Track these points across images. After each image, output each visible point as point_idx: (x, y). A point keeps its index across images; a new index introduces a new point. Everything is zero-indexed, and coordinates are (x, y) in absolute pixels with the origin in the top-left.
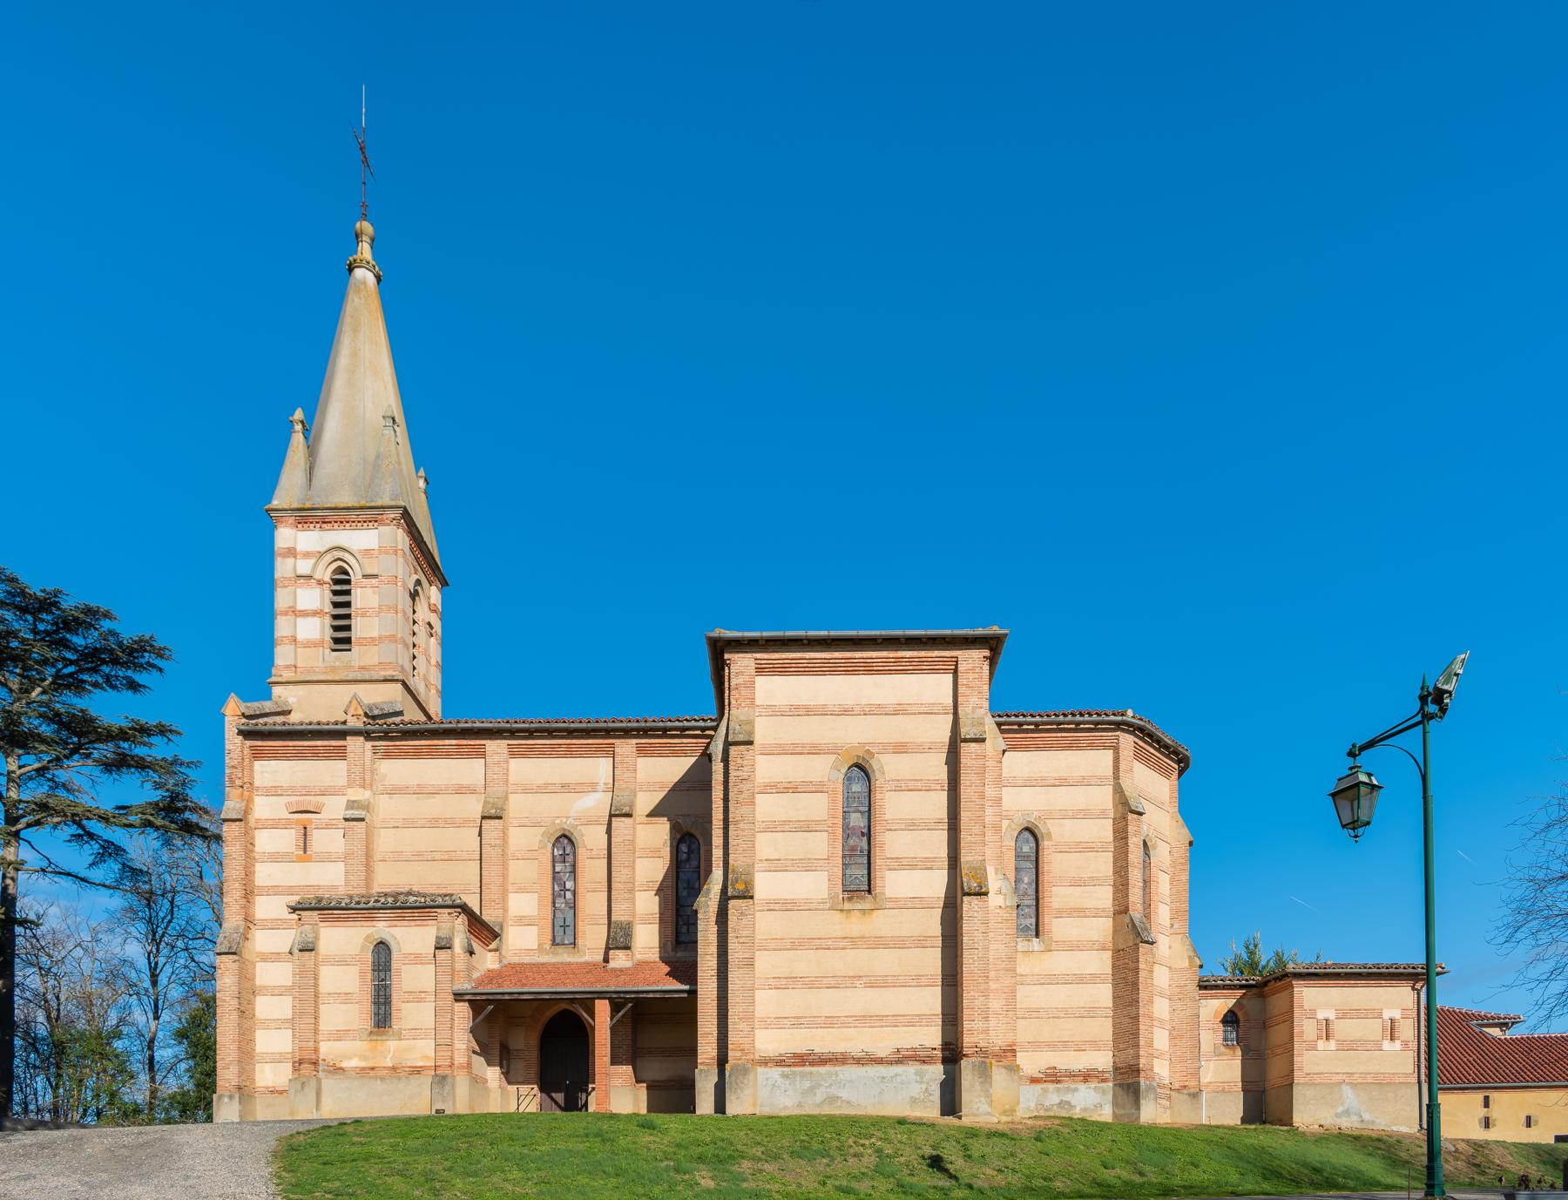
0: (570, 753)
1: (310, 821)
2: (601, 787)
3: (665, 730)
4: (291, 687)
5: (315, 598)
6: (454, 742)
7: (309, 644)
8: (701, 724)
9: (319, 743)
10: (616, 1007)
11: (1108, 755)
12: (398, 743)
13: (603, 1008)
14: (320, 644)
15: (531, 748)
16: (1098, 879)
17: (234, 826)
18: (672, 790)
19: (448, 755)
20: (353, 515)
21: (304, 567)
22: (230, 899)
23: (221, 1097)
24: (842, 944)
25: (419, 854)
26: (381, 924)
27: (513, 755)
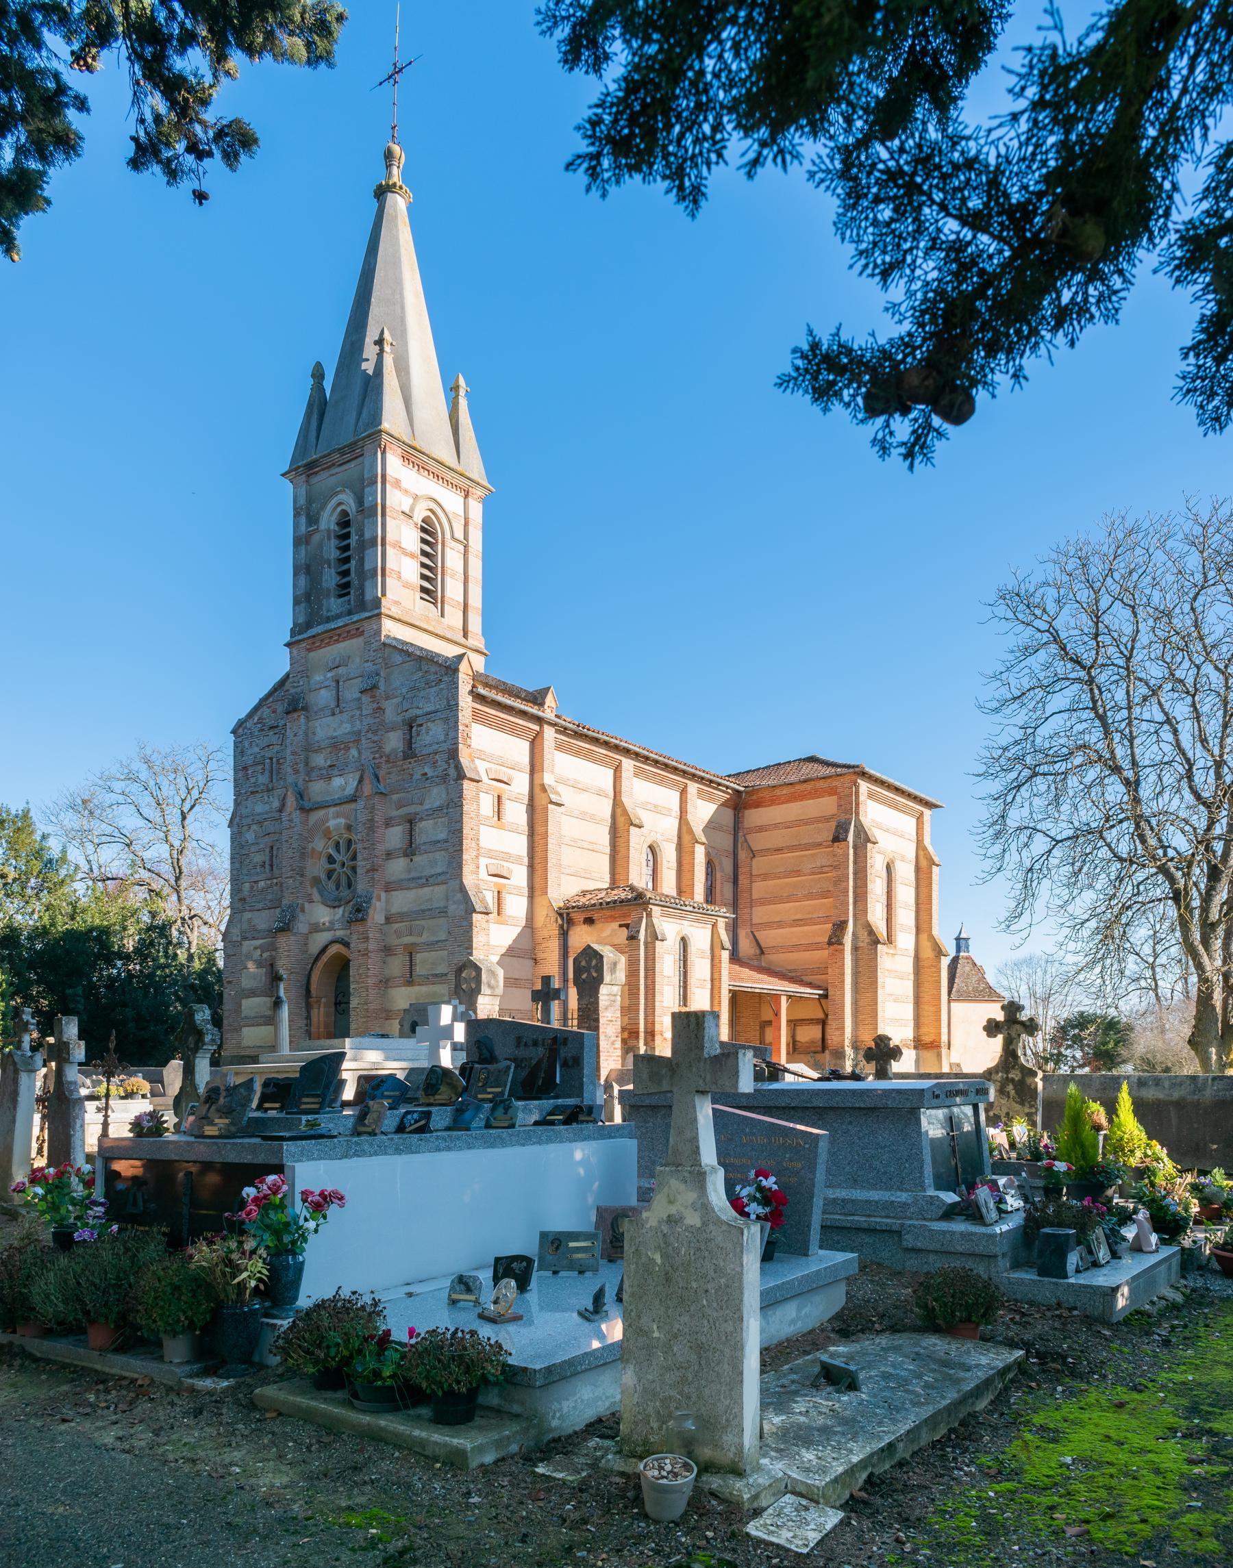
3: (711, 781)
4: (399, 625)
9: (521, 722)
13: (784, 999)
19: (594, 760)
20: (449, 475)
27: (636, 775)
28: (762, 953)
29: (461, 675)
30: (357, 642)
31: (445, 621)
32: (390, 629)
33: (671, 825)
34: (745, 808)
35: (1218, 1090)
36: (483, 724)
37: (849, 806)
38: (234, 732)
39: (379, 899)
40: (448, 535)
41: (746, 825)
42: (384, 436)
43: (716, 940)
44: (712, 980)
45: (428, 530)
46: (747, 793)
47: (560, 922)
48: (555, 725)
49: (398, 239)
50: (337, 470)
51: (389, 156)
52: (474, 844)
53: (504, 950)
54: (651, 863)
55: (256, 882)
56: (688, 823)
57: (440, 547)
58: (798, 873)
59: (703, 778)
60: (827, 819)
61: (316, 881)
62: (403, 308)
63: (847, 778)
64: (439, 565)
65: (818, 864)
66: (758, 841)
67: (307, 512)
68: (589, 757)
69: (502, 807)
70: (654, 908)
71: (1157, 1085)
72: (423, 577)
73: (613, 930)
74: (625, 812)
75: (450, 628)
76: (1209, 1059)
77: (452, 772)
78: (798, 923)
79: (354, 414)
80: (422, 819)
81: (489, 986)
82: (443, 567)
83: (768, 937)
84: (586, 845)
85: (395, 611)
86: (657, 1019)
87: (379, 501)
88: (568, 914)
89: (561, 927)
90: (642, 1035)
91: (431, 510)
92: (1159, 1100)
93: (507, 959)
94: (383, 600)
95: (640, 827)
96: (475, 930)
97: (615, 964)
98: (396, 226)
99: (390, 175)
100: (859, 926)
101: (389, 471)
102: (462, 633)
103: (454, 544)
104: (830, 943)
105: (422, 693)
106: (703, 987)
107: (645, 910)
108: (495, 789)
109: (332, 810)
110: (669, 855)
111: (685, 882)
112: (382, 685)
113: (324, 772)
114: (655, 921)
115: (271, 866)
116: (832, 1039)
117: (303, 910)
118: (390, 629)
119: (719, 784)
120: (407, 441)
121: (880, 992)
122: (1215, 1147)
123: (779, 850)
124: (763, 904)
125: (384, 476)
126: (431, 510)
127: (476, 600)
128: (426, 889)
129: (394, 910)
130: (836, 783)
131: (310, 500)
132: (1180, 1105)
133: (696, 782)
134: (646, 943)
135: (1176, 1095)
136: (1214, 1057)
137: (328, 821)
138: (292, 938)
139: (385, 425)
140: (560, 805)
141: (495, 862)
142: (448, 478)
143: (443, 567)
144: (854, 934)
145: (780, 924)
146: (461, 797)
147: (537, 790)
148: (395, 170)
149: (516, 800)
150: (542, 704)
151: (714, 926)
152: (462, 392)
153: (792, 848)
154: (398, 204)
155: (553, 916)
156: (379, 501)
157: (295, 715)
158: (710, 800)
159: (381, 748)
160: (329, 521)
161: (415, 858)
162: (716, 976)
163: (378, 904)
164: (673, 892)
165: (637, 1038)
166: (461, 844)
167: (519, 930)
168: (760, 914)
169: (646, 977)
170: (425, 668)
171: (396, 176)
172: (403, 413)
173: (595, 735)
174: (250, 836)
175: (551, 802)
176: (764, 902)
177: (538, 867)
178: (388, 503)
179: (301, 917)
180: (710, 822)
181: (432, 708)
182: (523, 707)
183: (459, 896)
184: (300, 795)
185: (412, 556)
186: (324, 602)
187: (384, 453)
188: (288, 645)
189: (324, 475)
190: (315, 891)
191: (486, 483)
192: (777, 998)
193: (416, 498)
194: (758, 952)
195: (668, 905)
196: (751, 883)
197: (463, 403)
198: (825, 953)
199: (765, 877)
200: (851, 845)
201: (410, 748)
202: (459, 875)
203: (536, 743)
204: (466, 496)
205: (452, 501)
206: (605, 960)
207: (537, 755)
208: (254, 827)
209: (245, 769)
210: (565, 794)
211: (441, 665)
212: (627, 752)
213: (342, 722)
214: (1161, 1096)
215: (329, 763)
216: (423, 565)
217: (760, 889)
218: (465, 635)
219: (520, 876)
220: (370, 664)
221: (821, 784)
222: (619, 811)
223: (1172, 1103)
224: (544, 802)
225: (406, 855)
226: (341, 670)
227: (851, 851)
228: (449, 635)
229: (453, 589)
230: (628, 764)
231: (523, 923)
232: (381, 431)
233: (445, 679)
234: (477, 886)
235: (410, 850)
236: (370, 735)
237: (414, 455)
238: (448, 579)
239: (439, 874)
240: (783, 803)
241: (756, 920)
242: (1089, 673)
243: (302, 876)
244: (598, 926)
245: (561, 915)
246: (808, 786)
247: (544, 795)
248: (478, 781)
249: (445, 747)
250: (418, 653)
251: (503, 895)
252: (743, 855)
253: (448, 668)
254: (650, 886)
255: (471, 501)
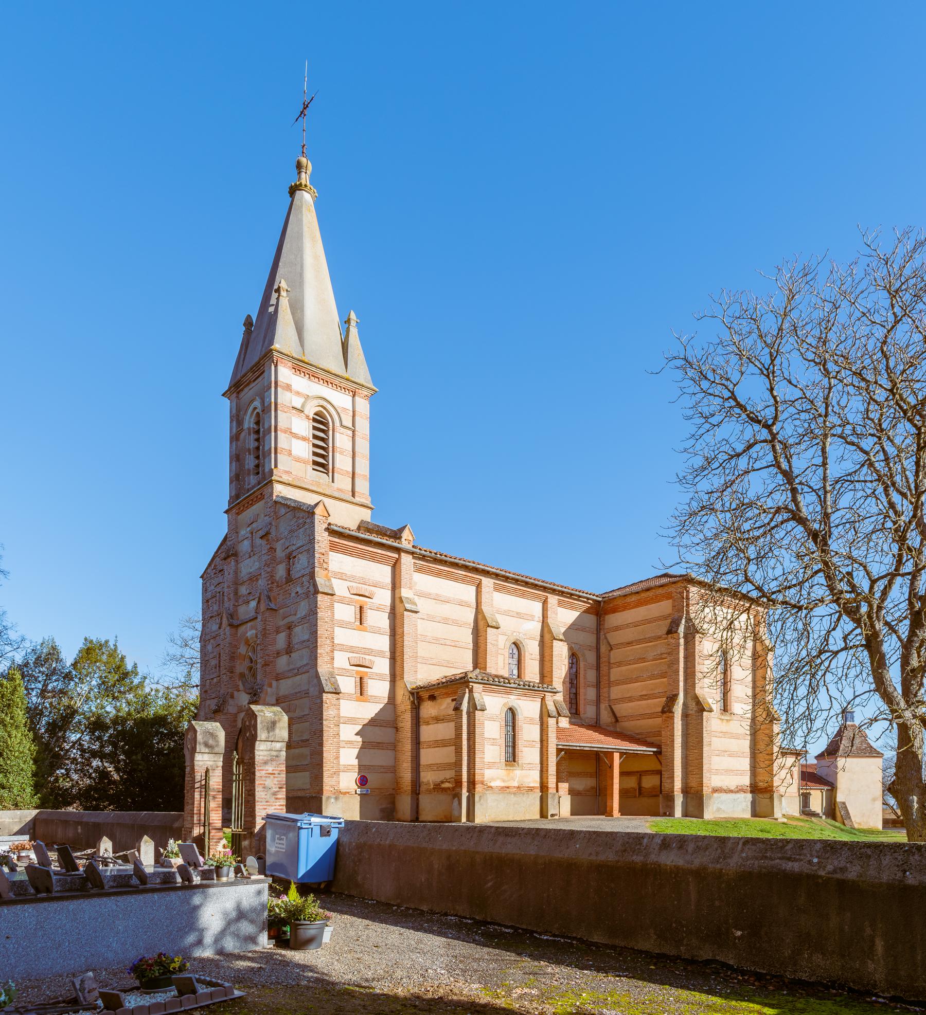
0: (523, 595)
1: (366, 603)
2: (537, 619)
3: (572, 595)
4: (289, 488)
5: (304, 427)
6: (464, 573)
7: (298, 460)
8: (588, 596)
9: (379, 551)
10: (622, 754)
11: (472, 589)
12: (431, 565)
13: (616, 756)
14: (305, 462)
15: (504, 587)
16: (372, 650)
17: (326, 597)
18: (569, 628)
19: (456, 579)
20: (337, 381)
21: (298, 402)
22: (323, 652)
23: (328, 798)
24: (721, 735)
25: (437, 639)
26: (512, 697)
27: (496, 589)
28: (617, 721)
29: (316, 517)
30: (260, 504)
31: (335, 485)
32: (279, 490)
33: (535, 627)
34: (606, 614)
35: (747, 858)
36: (338, 551)
37: (681, 605)
38: (202, 577)
39: (270, 686)
40: (337, 423)
41: (606, 626)
42: (275, 353)
43: (544, 710)
44: (542, 741)
45: (321, 423)
46: (604, 602)
47: (412, 699)
48: (412, 553)
49: (302, 220)
50: (253, 385)
51: (299, 166)
52: (328, 642)
53: (366, 722)
54: (516, 656)
55: (212, 679)
56: (548, 626)
57: (331, 433)
58: (643, 660)
59: (563, 592)
60: (665, 618)
61: (242, 675)
62: (302, 267)
63: (679, 584)
64: (331, 445)
65: (659, 652)
66: (615, 638)
67: (237, 418)
68: (448, 576)
69: (364, 615)
70: (475, 685)
71: (680, 848)
72: (315, 454)
73: (448, 704)
74: (484, 618)
75: (339, 490)
76: (911, 807)
77: (311, 589)
78: (643, 697)
79: (261, 343)
80: (295, 626)
81: (206, 745)
82: (333, 447)
83: (622, 709)
84: (448, 642)
85: (285, 478)
86: (477, 771)
87: (273, 400)
88: (418, 693)
89: (413, 703)
90: (465, 785)
91: (322, 406)
92: (677, 868)
93: (370, 728)
94: (275, 471)
95: (497, 628)
96: (325, 706)
97: (274, 723)
98: (301, 212)
99: (300, 178)
100: (689, 699)
101: (280, 378)
102: (351, 494)
103: (343, 430)
104: (663, 712)
105: (296, 534)
106: (533, 747)
107: (468, 687)
108: (357, 601)
109: (249, 624)
110: (532, 649)
111: (546, 669)
112: (273, 533)
113: (245, 598)
114: (476, 695)
115: (219, 667)
116: (666, 786)
117: (232, 697)
118: (279, 490)
119: (580, 597)
120: (295, 355)
121: (705, 749)
122: (739, 933)
123: (629, 644)
124: (618, 684)
125: (276, 383)
126: (322, 406)
127: (363, 467)
128: (298, 677)
129: (281, 693)
130: (671, 589)
131: (239, 409)
132: (700, 874)
133: (558, 595)
134: (468, 713)
135: (697, 862)
136: (916, 806)
137: (246, 633)
138: (223, 717)
139: (276, 346)
140: (416, 612)
141: (355, 655)
142: (337, 382)
143: (333, 447)
144: (685, 704)
145: (630, 699)
146: (316, 607)
147: (397, 601)
148: (303, 175)
149: (378, 609)
150: (400, 538)
151: (543, 699)
152: (353, 323)
153: (639, 642)
154: (306, 198)
155: (407, 694)
156: (273, 400)
157: (229, 560)
158: (572, 608)
159: (272, 576)
160: (249, 422)
161: (293, 655)
162: (544, 738)
163: (269, 690)
164: (536, 679)
165: (461, 786)
166: (317, 642)
167: (382, 706)
168: (616, 692)
169: (469, 739)
170: (298, 515)
171: (305, 178)
172: (295, 337)
173: (452, 560)
174: (209, 648)
175: (406, 610)
176: (619, 683)
177: (398, 659)
178: (279, 401)
179: (231, 701)
180: (572, 624)
181: (301, 544)
182: (378, 540)
183: (315, 681)
184: (231, 616)
185: (304, 439)
186: (246, 479)
187: (276, 366)
188: (226, 512)
189: (246, 390)
190: (240, 683)
191: (371, 386)
192: (609, 755)
193: (307, 397)
194: (613, 720)
195: (497, 683)
196: (609, 669)
197: (354, 331)
198: (659, 721)
199: (620, 664)
200: (682, 635)
201: (289, 574)
202: (315, 665)
203: (396, 567)
204: (354, 396)
205: (341, 400)
206: (259, 720)
207: (397, 576)
208: (212, 641)
209: (208, 601)
210: (422, 605)
211: (305, 511)
212: (486, 573)
213: (254, 561)
214: (681, 862)
215: (248, 592)
216: (315, 446)
217: (615, 673)
218: (353, 495)
219: (383, 666)
220: (267, 517)
221: (660, 591)
222: (480, 617)
223: (691, 872)
224: (402, 609)
225: (287, 653)
226: (254, 525)
227: (682, 641)
228: (342, 497)
229: (342, 462)
230: (487, 582)
231: (386, 701)
232: (272, 350)
233: (308, 521)
234: (332, 675)
235: (289, 650)
236: (266, 568)
237: (301, 366)
238: (337, 456)
239: (305, 665)
240: (633, 608)
241: (613, 696)
242: (771, 432)
243: (232, 672)
244: (439, 701)
245: (412, 694)
246: (650, 594)
247: (401, 605)
248: (332, 595)
249: (307, 571)
250: (293, 505)
251: (365, 680)
252: (603, 648)
253: (308, 512)
254: (515, 672)
255: (357, 398)
